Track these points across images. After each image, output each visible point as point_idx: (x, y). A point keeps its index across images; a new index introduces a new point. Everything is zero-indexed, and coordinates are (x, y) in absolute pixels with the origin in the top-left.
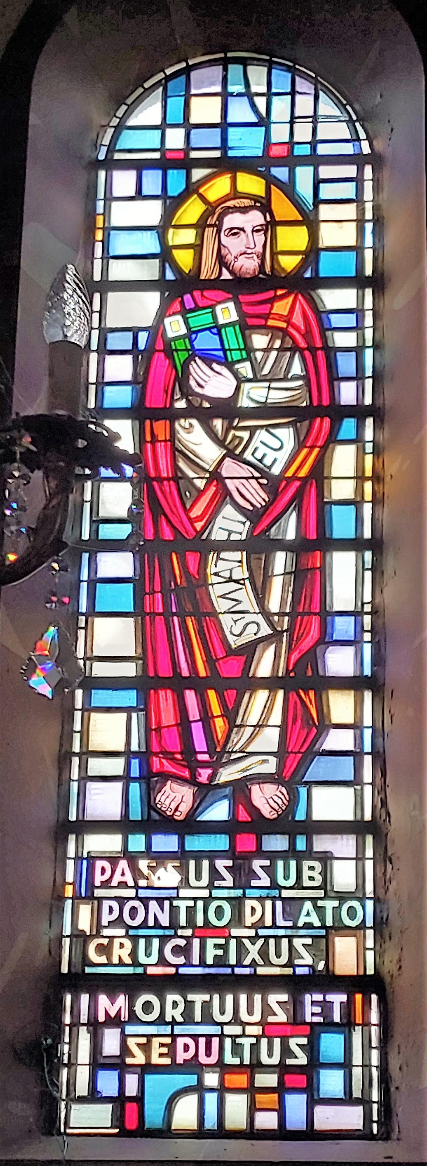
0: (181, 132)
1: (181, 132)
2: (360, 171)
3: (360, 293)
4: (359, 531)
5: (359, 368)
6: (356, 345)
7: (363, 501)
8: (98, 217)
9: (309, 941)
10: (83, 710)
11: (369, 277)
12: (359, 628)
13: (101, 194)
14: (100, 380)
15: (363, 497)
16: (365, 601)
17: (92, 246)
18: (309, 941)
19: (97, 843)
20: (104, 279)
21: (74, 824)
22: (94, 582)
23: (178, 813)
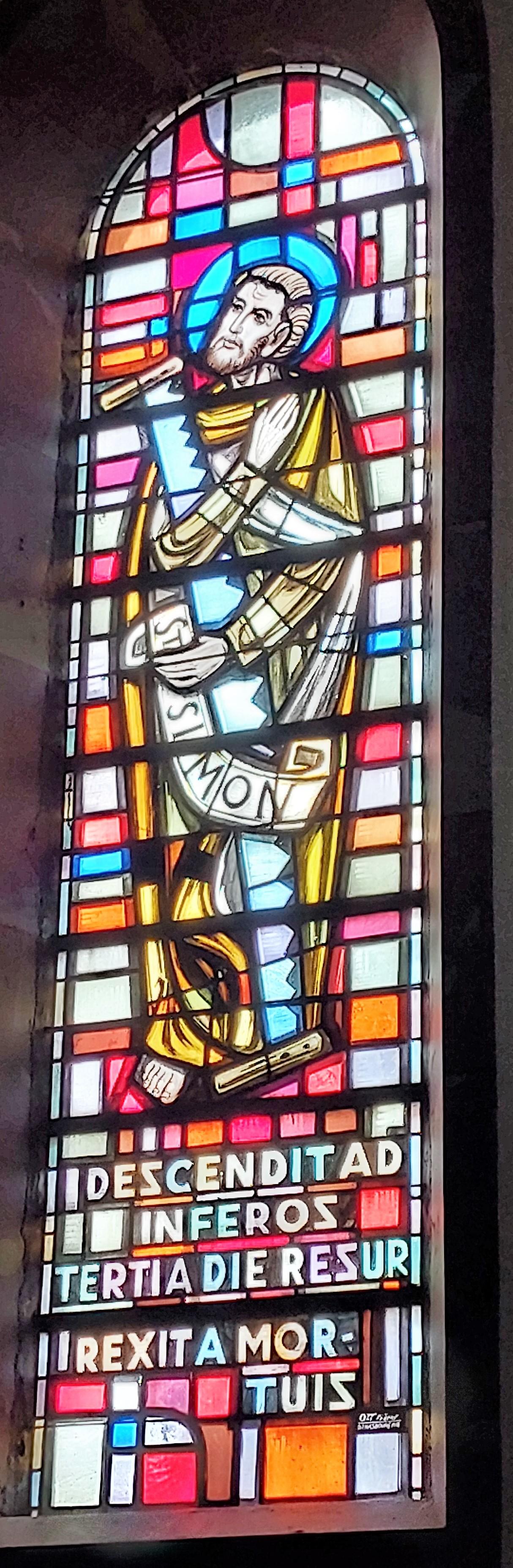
0: (133, 1404)
1: (133, 1404)
2: (404, 922)
3: (411, 208)
4: (405, 695)
5: (407, 486)
6: (398, 1082)
7: (410, 1406)
8: (83, 387)
9: (333, 1199)
10: (71, 880)
11: (416, 1085)
12: (408, 467)
13: (75, 635)
14: (53, 1372)
15: (414, 272)
16: (414, 1350)
17: (63, 713)
18: (333, 1199)
19: (79, 1145)
20: (72, 931)
21: (65, 939)
22: (99, 308)
23: (165, 1094)
